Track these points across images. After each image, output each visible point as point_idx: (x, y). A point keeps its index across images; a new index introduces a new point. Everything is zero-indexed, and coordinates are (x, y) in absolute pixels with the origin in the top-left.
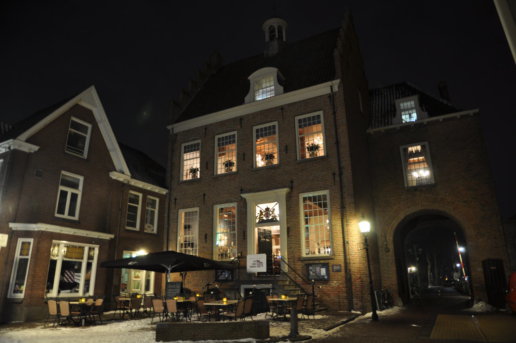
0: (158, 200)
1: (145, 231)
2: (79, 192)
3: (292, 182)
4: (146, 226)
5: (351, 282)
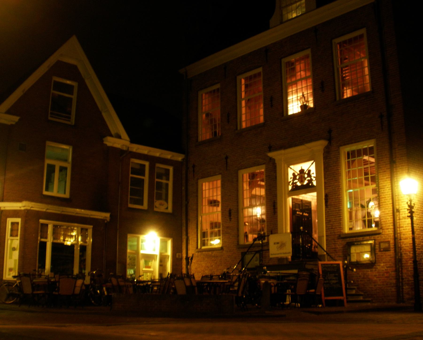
0: (171, 169)
1: (155, 209)
3: (330, 131)
4: (157, 203)
5: (401, 264)
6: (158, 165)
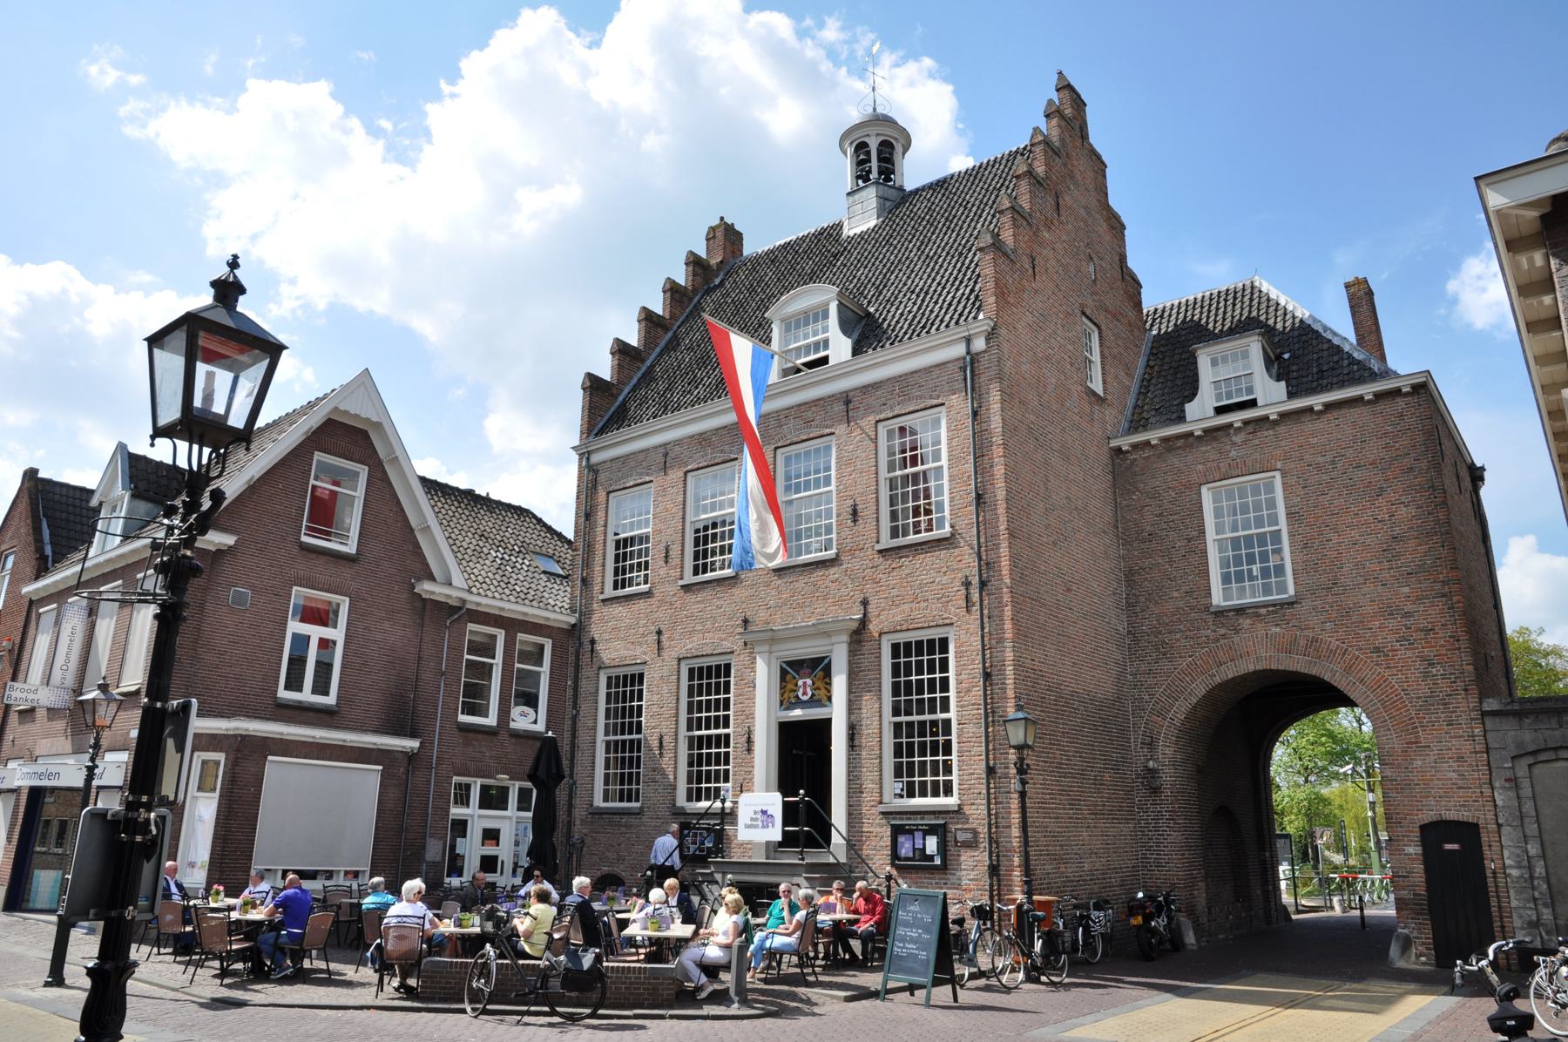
0: (548, 645)
2: (337, 634)
4: (516, 711)
6: (520, 636)
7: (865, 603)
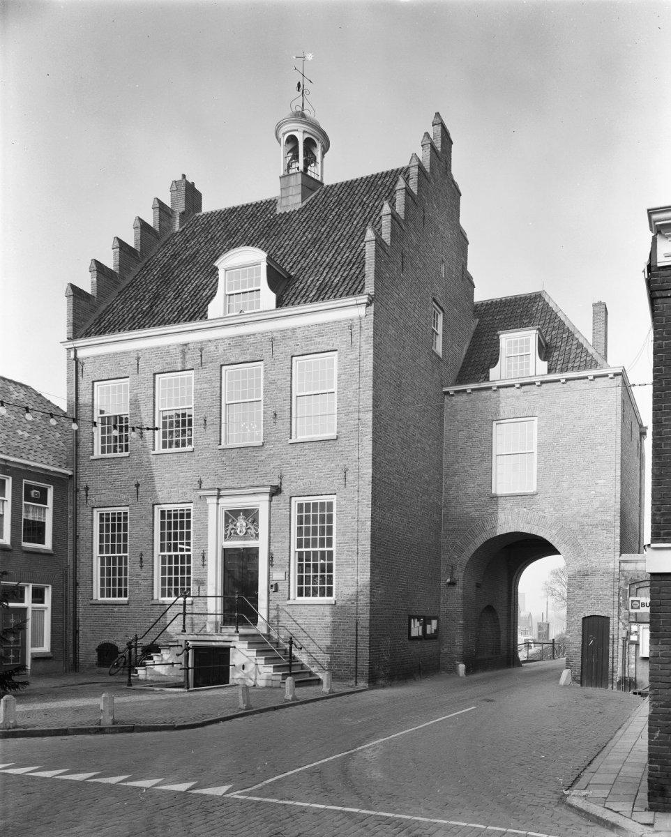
7: (281, 477)
